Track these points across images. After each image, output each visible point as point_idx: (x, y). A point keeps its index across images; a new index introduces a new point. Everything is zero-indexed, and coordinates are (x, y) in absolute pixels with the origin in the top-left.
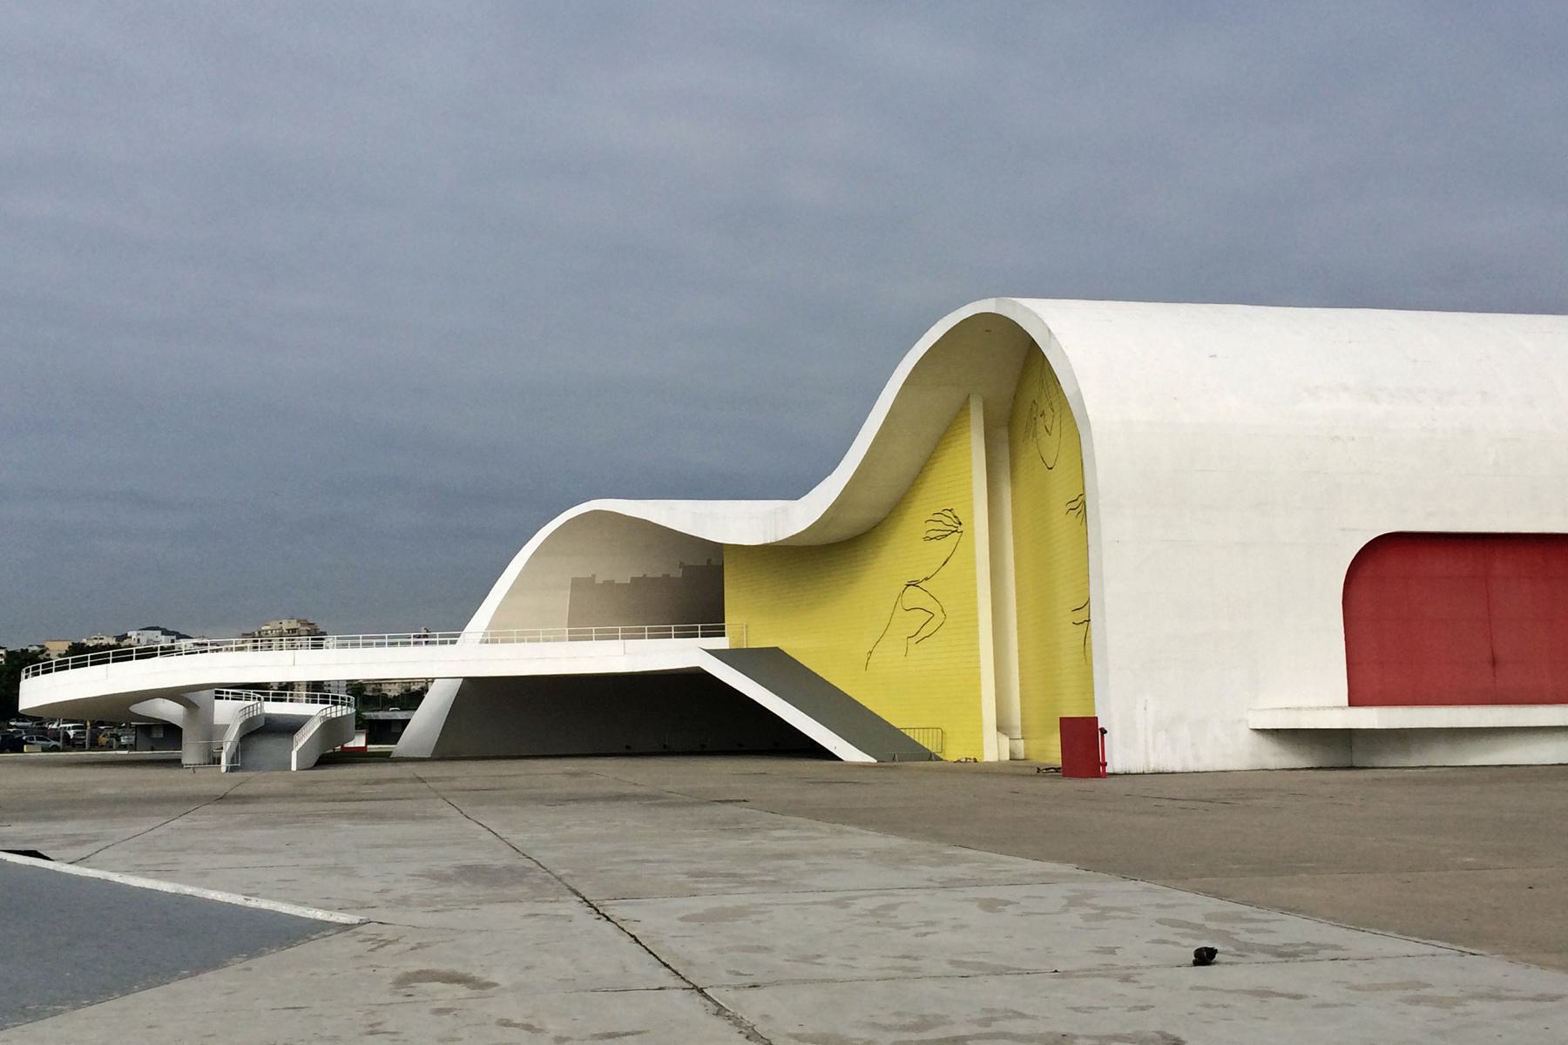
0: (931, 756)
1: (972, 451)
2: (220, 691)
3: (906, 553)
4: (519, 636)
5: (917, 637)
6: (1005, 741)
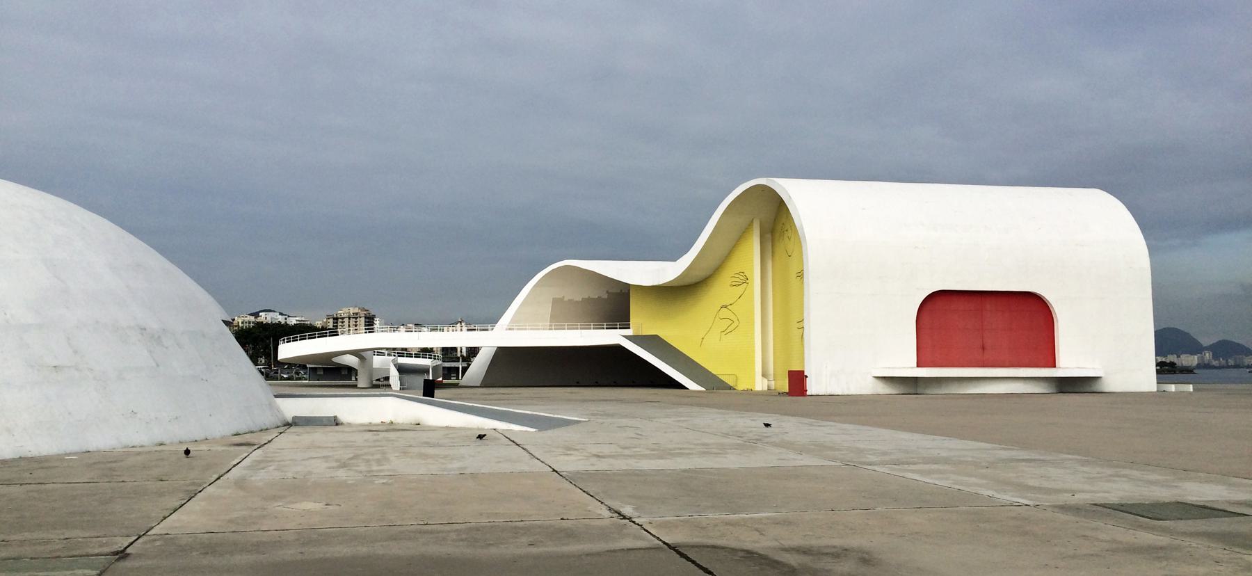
0: (730, 388)
1: (754, 245)
2: (379, 352)
3: (721, 292)
4: (526, 326)
5: (726, 332)
6: (766, 381)
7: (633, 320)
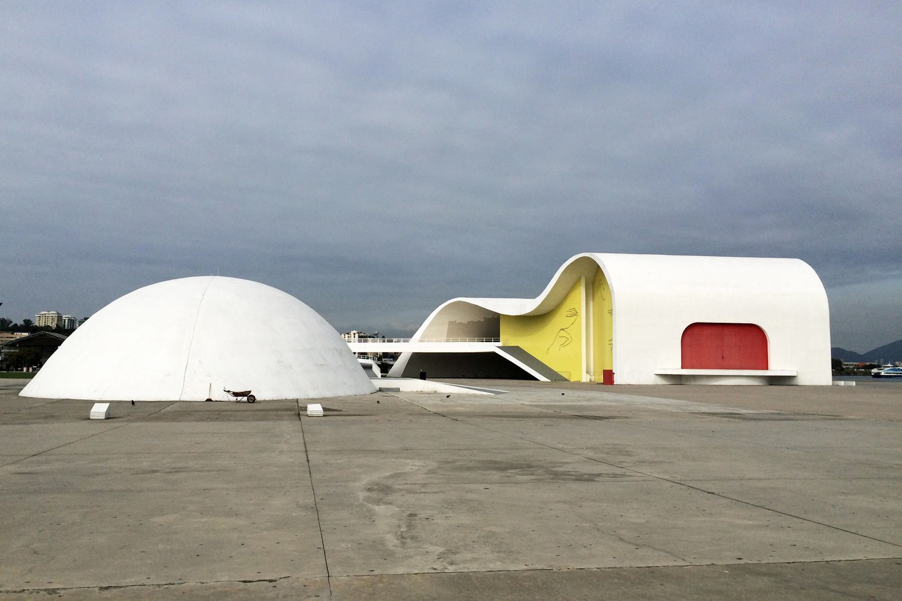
0: (566, 380)
1: (581, 292)
3: (560, 320)
4: (433, 337)
5: (563, 345)
7: (502, 337)
